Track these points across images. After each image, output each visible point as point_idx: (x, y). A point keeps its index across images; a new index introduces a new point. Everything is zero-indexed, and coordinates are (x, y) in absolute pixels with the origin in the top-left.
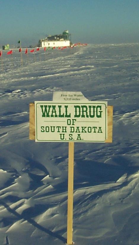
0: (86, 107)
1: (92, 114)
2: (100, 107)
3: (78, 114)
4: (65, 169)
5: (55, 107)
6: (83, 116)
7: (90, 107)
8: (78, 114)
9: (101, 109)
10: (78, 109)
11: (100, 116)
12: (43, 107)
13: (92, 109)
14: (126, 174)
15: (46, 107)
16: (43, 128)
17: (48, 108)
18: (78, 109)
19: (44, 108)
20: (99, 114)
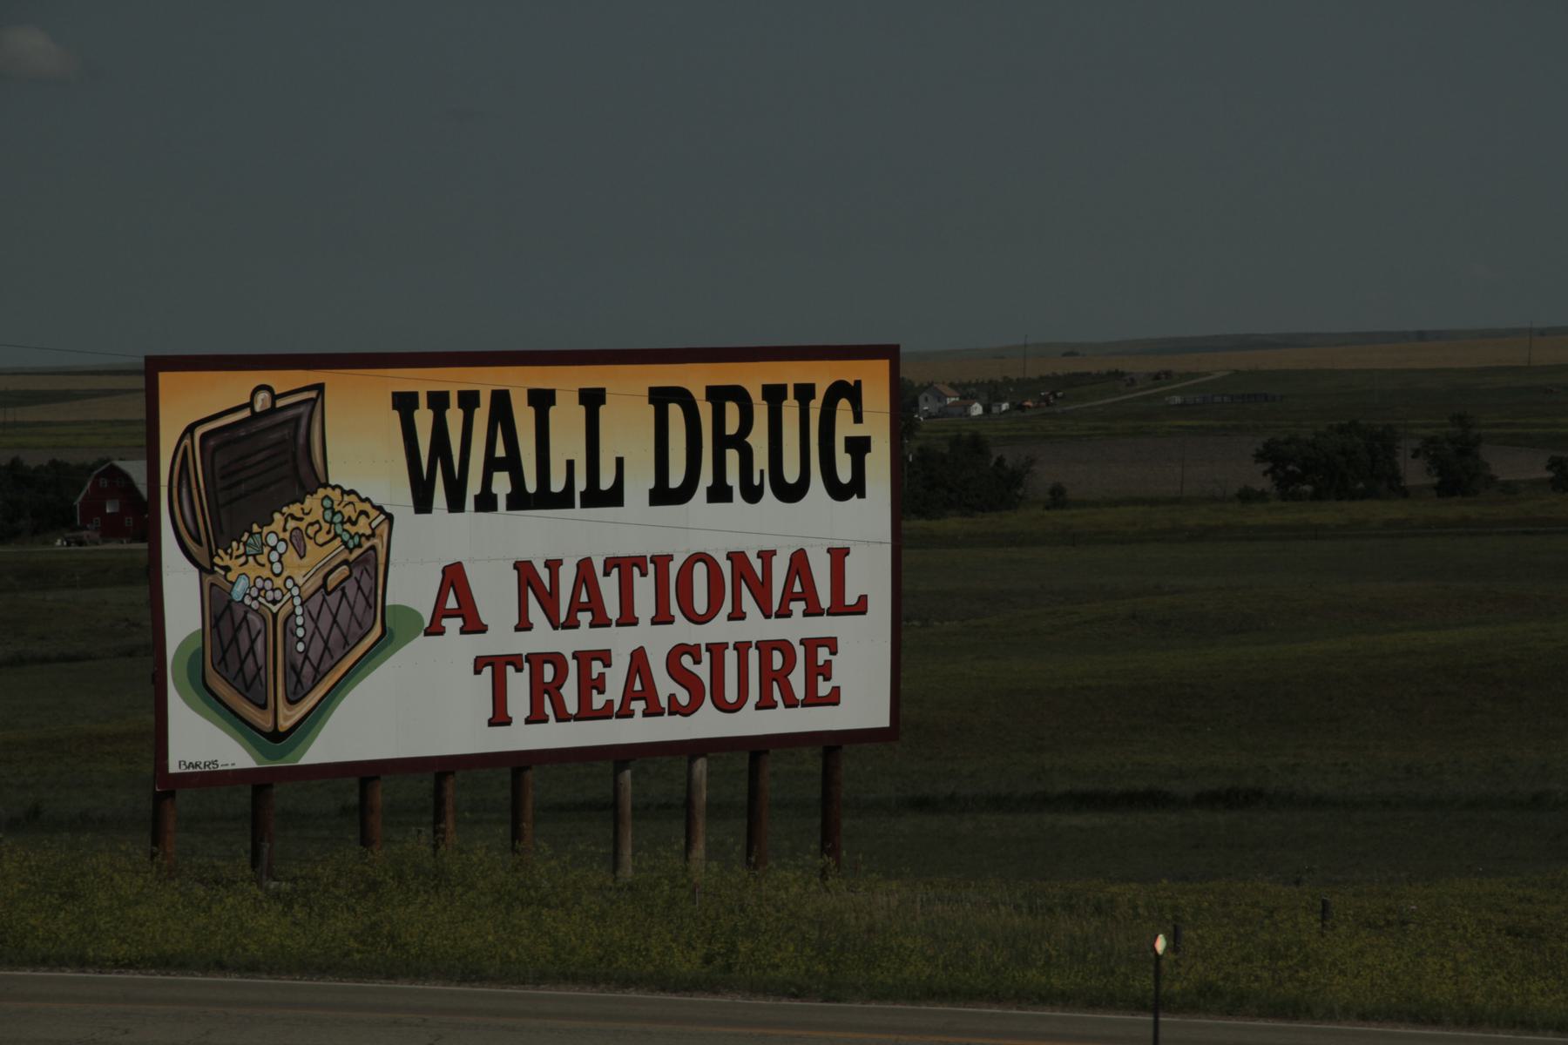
0: (739, 395)
1: (791, 474)
2: (852, 392)
3: (676, 479)
4: (1323, 935)
5: (603, 402)
6: (720, 493)
7: (774, 395)
8: (676, 479)
9: (858, 418)
10: (675, 412)
11: (857, 487)
12: (447, 406)
13: (790, 410)
14: (820, 678)
15: (438, 402)
16: (687, 661)
17: (454, 417)
18: (675, 412)
19: (424, 419)
20: (844, 474)
